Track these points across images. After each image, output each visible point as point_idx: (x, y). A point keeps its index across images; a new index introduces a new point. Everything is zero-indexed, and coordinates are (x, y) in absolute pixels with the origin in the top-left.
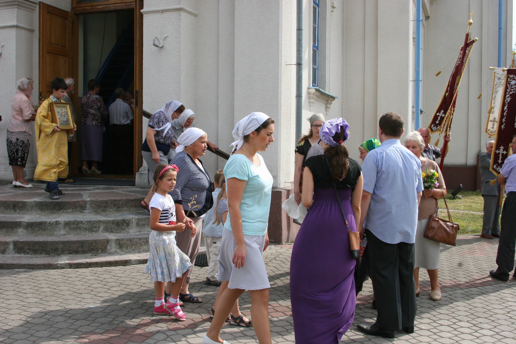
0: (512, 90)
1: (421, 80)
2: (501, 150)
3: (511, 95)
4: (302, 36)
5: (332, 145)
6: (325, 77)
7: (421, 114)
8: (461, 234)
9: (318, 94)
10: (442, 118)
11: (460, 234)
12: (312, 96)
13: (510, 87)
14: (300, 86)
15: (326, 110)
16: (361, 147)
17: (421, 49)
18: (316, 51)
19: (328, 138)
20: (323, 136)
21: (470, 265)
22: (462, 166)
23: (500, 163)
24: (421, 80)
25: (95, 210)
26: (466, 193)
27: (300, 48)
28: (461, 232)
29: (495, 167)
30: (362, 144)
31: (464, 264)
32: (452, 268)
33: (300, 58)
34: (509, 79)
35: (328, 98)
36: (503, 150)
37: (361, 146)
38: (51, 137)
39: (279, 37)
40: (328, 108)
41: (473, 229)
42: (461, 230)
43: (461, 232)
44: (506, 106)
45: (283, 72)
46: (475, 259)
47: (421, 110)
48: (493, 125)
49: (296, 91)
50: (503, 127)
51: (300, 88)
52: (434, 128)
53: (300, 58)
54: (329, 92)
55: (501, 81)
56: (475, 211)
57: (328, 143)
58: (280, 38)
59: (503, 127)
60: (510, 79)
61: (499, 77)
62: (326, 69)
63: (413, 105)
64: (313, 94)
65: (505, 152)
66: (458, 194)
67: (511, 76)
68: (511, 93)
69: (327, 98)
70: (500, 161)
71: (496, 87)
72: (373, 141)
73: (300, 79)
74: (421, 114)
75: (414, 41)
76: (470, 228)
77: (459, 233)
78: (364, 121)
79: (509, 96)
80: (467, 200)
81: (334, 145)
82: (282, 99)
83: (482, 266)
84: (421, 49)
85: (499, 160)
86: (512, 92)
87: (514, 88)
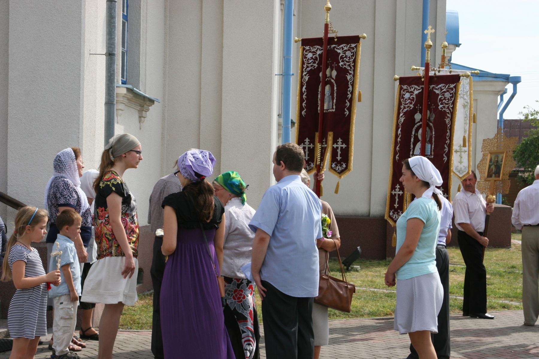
0: (406, 106)
1: (293, 75)
2: (340, 143)
3: (405, 114)
4: (115, 11)
5: (192, 179)
6: (139, 67)
7: (292, 127)
8: (353, 318)
9: (130, 95)
11: (351, 318)
12: (122, 99)
13: (404, 103)
14: (111, 89)
15: (140, 122)
16: (215, 182)
17: (294, 15)
18: (125, 23)
19: (189, 172)
20: (184, 168)
21: (360, 352)
22: (362, 216)
23: (339, 160)
24: (293, 75)
26: (368, 262)
27: (112, 29)
28: (352, 315)
30: (217, 178)
32: (335, 354)
33: (112, 44)
35: (144, 100)
36: (341, 143)
37: (215, 180)
39: (81, 12)
40: (142, 118)
41: (371, 310)
42: (353, 311)
43: (352, 315)
44: (400, 129)
45: (85, 65)
46: (370, 346)
47: (292, 120)
49: (106, 95)
50: (303, 113)
51: (112, 91)
52: (338, 167)
53: (112, 44)
54: (145, 92)
56: (379, 288)
57: (188, 177)
58: (83, 14)
59: (303, 113)
62: (141, 53)
63: (279, 112)
64: (123, 96)
65: (401, 193)
66: (354, 263)
67: (405, 87)
68: (309, 69)
69: (143, 102)
72: (231, 174)
73: (112, 78)
74: (292, 127)
75: (281, 4)
76: (367, 310)
77: (350, 316)
78: (199, 139)
79: (307, 74)
80: (369, 273)
81: (194, 180)
82: (85, 106)
83: (377, 353)
84: (294, 15)
85: (338, 157)
86: (310, 68)
87: (311, 63)
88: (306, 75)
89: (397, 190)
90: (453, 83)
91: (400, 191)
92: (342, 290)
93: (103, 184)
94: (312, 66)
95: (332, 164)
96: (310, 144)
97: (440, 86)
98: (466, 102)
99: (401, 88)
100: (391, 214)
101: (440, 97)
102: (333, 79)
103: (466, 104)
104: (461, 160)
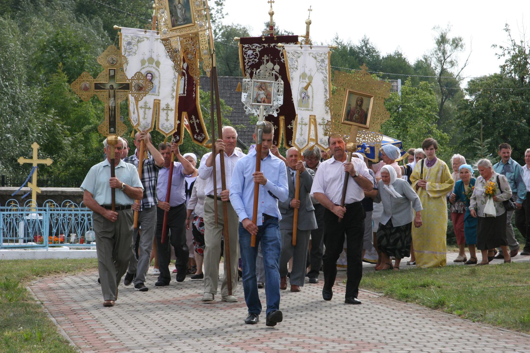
2: (194, 119)
29: (195, 137)
34: (244, 49)
48: (167, 114)
52: (199, 138)
55: (131, 46)
60: (245, 49)
61: (129, 40)
65: (198, 121)
67: (246, 46)
79: (249, 67)
86: (252, 63)
87: (252, 58)
88: (248, 69)
91: (196, 120)
93: (133, 158)
94: (253, 61)
95: (194, 136)
96: (196, 120)
99: (243, 47)
102: (184, 70)
104: (167, 117)
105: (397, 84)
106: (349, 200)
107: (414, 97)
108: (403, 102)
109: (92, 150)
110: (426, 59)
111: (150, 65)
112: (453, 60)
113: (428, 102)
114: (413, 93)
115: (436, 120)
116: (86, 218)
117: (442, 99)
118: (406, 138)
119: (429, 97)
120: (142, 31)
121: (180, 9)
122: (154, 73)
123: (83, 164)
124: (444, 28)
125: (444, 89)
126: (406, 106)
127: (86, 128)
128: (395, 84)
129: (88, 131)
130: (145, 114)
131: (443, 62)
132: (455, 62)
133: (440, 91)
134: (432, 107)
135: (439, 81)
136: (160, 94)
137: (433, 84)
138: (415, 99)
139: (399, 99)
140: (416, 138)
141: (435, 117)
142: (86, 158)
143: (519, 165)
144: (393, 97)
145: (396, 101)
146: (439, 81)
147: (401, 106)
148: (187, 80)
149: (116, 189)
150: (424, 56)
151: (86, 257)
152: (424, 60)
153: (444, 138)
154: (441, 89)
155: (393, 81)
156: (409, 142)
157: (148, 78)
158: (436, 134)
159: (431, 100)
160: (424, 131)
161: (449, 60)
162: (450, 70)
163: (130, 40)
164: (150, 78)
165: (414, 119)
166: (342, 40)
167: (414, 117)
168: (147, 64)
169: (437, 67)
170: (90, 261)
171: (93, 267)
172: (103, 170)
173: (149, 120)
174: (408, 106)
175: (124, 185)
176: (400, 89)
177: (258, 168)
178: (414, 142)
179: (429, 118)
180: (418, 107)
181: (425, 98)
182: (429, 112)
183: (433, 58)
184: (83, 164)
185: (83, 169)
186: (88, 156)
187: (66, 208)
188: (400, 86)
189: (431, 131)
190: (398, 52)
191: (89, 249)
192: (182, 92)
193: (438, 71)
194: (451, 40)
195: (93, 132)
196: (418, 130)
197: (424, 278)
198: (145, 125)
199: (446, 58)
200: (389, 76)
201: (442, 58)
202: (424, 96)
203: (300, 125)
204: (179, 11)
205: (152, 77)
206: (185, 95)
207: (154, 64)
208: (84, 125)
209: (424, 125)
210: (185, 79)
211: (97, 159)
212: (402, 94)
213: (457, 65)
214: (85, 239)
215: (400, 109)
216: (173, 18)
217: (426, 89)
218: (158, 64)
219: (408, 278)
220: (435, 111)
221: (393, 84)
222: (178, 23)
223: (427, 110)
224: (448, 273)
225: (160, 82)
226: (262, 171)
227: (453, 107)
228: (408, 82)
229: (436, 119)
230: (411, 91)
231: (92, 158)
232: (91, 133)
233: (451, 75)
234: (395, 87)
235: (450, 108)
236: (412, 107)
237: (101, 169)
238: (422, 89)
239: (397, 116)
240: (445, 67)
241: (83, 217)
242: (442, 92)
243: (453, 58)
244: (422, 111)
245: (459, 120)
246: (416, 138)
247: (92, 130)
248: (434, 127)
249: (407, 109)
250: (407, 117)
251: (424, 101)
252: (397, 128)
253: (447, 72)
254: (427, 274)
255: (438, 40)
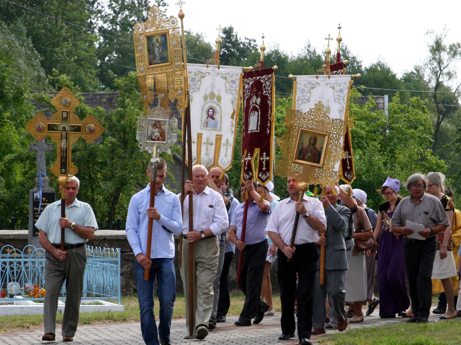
2: (264, 156)
10: (268, 163)
25: (252, 43)
31: (398, 225)
38: (76, 148)
52: (263, 176)
55: (195, 82)
70: (349, 168)
71: (299, 103)
89: (264, 156)
90: (270, 74)
91: (266, 157)
92: (268, 274)
95: (259, 174)
97: (264, 77)
98: (234, 98)
100: (260, 175)
101: (264, 85)
102: (257, 105)
103: (234, 100)
105: (384, 101)
106: (298, 241)
107: (404, 117)
108: (391, 123)
109: (16, 184)
110: (418, 71)
111: (212, 100)
112: (451, 71)
113: (421, 122)
114: (402, 111)
115: (430, 144)
116: (8, 267)
117: (439, 119)
118: (394, 166)
119: (422, 116)
120: (204, 66)
121: (158, 48)
122: (215, 109)
123: (4, 202)
124: (439, 32)
125: (441, 106)
126: (395, 128)
127: (8, 157)
128: (381, 101)
129: (11, 162)
130: (207, 150)
131: (439, 73)
132: (453, 73)
133: (436, 109)
134: (425, 129)
135: (435, 97)
136: (222, 129)
137: (427, 100)
138: (405, 119)
139: (386, 119)
140: (406, 166)
141: (430, 141)
142: (8, 194)
143: (351, 188)
144: (378, 117)
145: (382, 122)
146: (435, 97)
147: (388, 127)
148: (261, 116)
149: (65, 229)
150: (416, 66)
151: (8, 314)
152: (415, 72)
153: (440, 165)
154: (437, 106)
155: (379, 98)
156: (398, 171)
157: (210, 113)
158: (431, 161)
159: (424, 120)
160: (416, 157)
161: (445, 71)
162: (446, 84)
163: (194, 77)
164: (212, 113)
165: (403, 144)
166: (314, 48)
167: (404, 141)
168: (208, 100)
169: (432, 80)
170: (13, 319)
171: (17, 327)
172: (56, 209)
173: (212, 156)
174: (396, 127)
175: (73, 225)
176: (387, 107)
177: (152, 203)
178: (404, 171)
179: (422, 140)
180: (408, 129)
181: (417, 117)
182: (422, 134)
183: (426, 69)
184: (4, 202)
185: (5, 208)
186: (11, 192)
187: (8, 255)
188: (386, 104)
189: (425, 157)
190: (380, 62)
191: (12, 304)
192: (255, 128)
193: (433, 84)
194: (448, 47)
195: (17, 162)
196: (408, 156)
197: (416, 336)
198: (207, 161)
199: (442, 69)
200: (371, 90)
201: (438, 69)
202: (416, 115)
203: (206, 145)
204: (156, 50)
205: (213, 112)
206: (258, 131)
207: (215, 99)
208: (5, 153)
209: (416, 150)
210: (258, 115)
211: (21, 195)
212: (389, 113)
213: (456, 77)
214: (7, 292)
215: (387, 131)
216: (150, 56)
217: (417, 106)
218: (219, 99)
219: (396, 336)
220: (431, 134)
221: (378, 102)
222: (155, 61)
223: (420, 131)
224: (445, 329)
225: (221, 117)
226: (156, 206)
227: (451, 128)
228: (396, 98)
229: (431, 143)
230: (399, 109)
231: (16, 194)
232: (14, 163)
233: (448, 89)
234: (382, 105)
235: (448, 129)
236: (401, 129)
237: (55, 208)
238: (413, 106)
239: (383, 140)
240: (440, 80)
241: (4, 265)
242: (438, 110)
243: (451, 68)
244: (413, 133)
245: (458, 144)
246: (406, 166)
247: (16, 160)
248: (428, 153)
249: (395, 132)
250: (395, 141)
251: (416, 122)
252: (384, 154)
253: (443, 85)
254: (419, 331)
255: (433, 47)
